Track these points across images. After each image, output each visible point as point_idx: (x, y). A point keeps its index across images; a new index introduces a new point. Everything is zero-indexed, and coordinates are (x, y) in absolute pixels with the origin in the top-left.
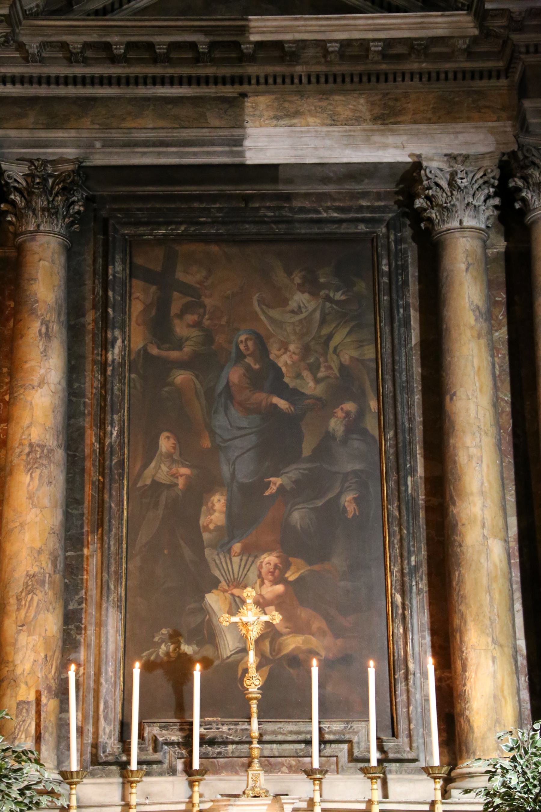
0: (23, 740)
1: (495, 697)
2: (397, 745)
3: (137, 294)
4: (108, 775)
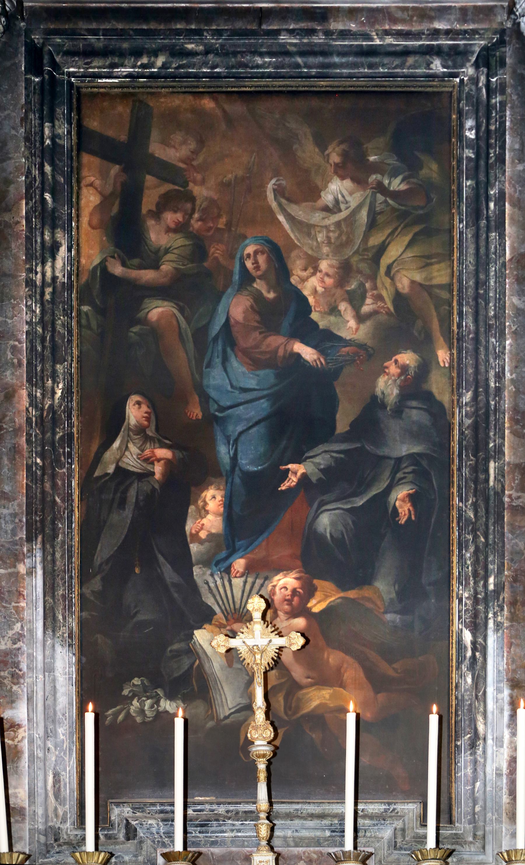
2: (456, 834)
3: (90, 176)
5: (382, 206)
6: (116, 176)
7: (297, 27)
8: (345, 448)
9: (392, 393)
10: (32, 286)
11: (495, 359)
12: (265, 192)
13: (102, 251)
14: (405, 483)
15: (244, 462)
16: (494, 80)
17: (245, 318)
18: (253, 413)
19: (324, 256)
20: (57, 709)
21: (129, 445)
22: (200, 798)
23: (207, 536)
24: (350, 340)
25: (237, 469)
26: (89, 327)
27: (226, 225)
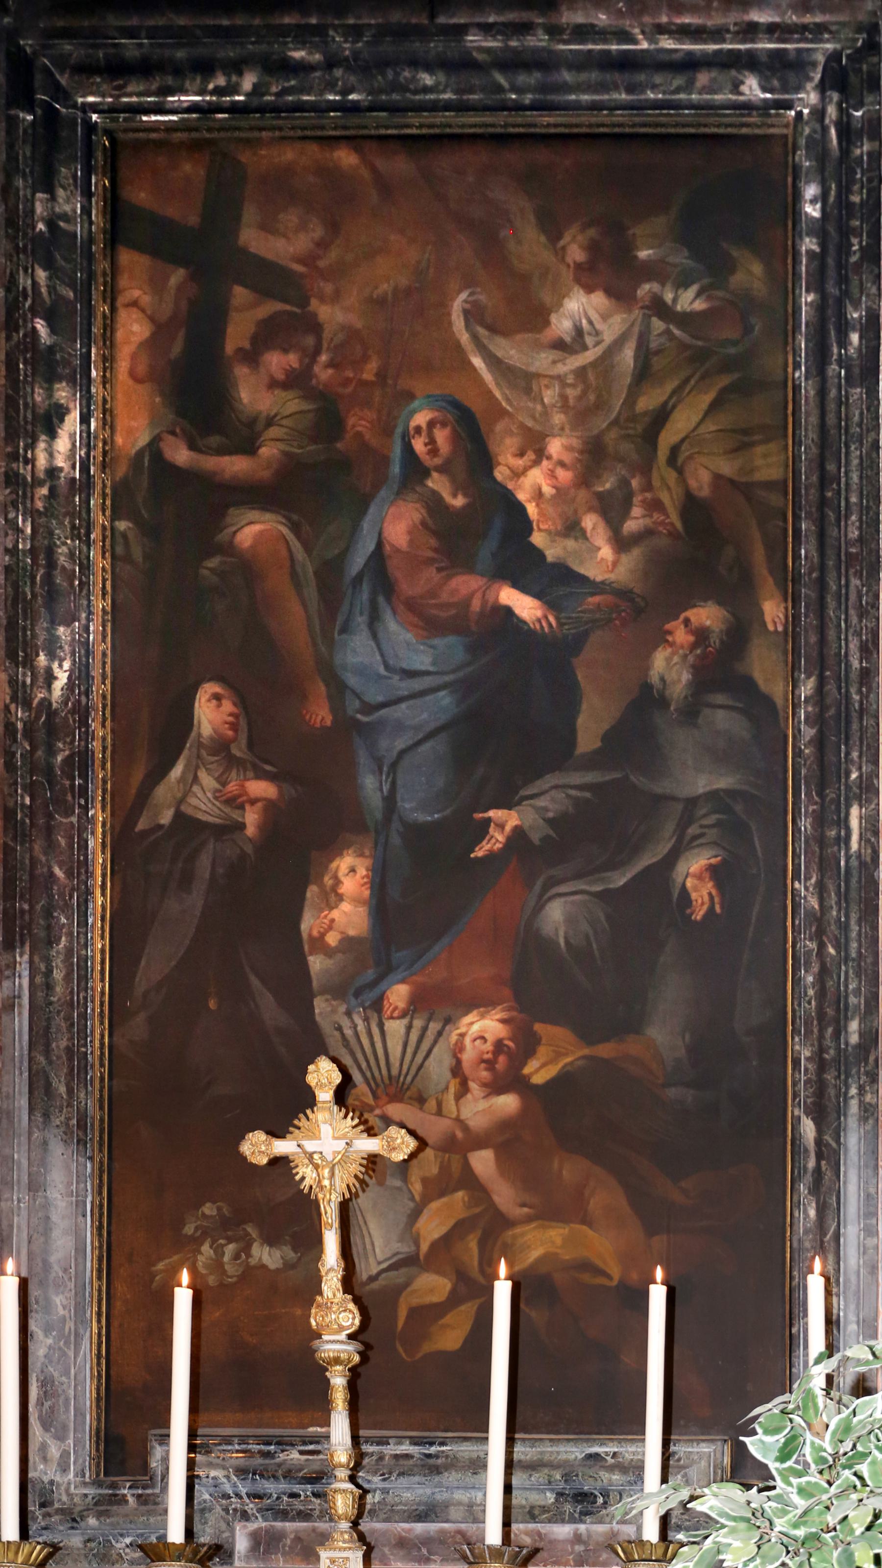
3: (133, 290)
5: (662, 340)
6: (180, 288)
7: (501, 19)
8: (594, 781)
9: (679, 680)
10: (18, 485)
11: (860, 617)
12: (449, 314)
13: (152, 424)
14: (702, 845)
15: (407, 806)
16: (859, 114)
17: (411, 542)
18: (425, 716)
19: (556, 431)
20: (53, 1259)
21: (199, 774)
22: (319, 1429)
23: (340, 941)
24: (603, 583)
25: (395, 817)
26: (127, 558)
27: (377, 375)
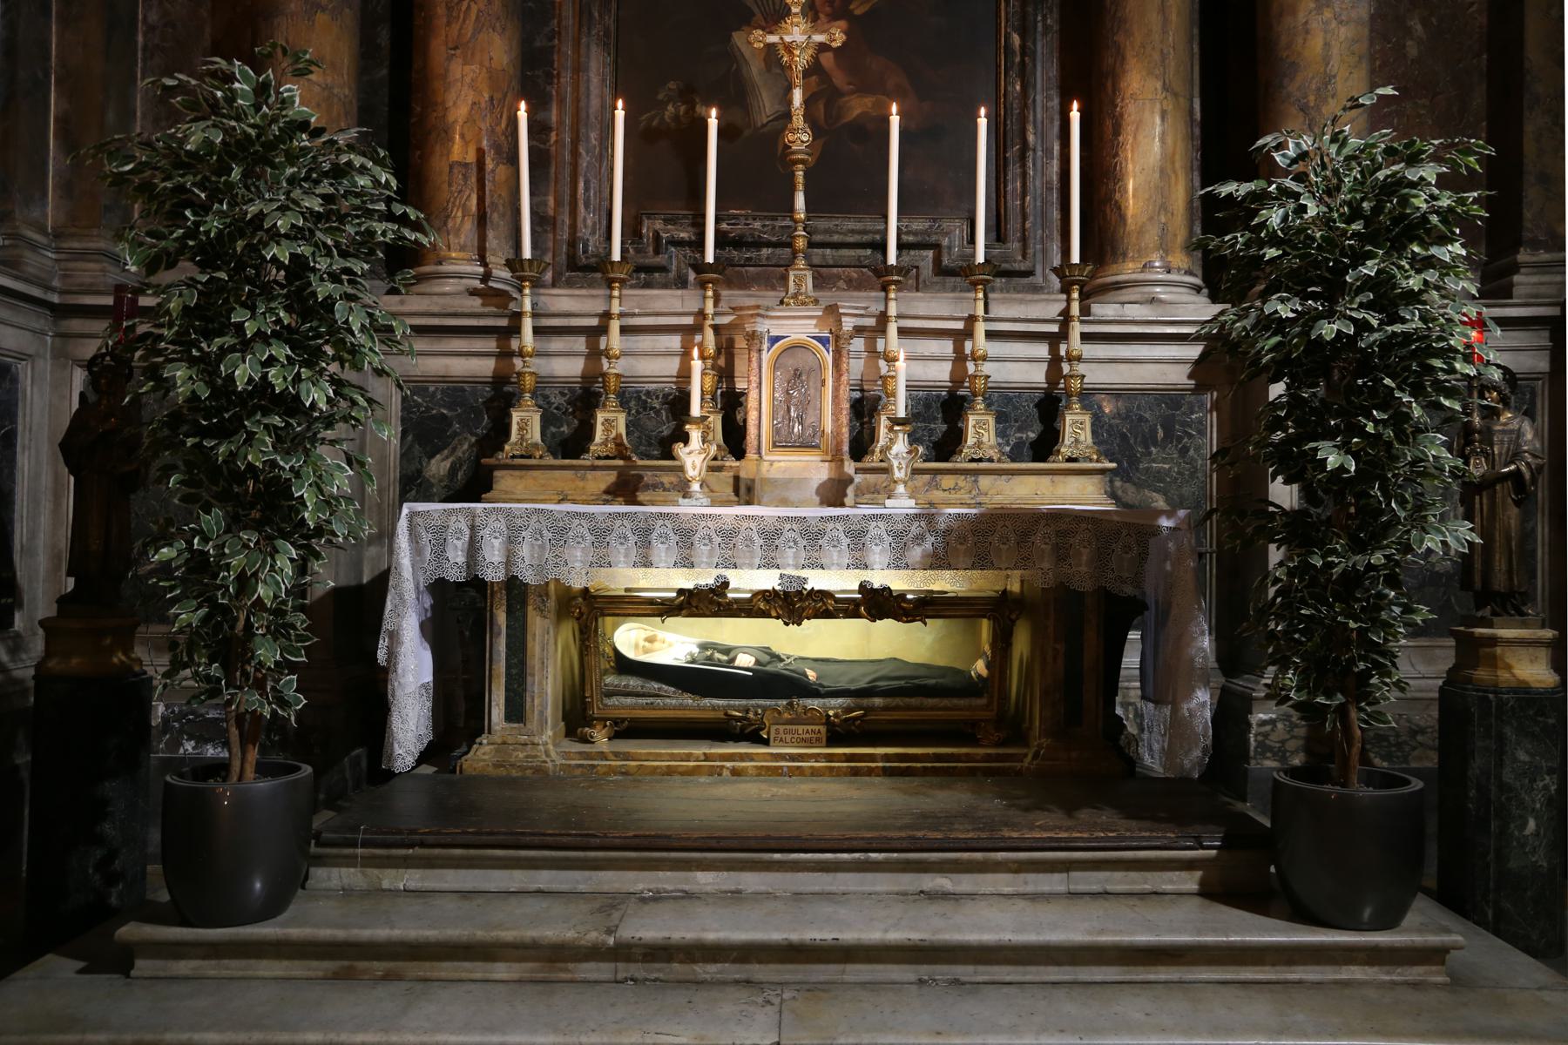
0: (459, 220)
1: (1162, 171)
4: (591, 285)
